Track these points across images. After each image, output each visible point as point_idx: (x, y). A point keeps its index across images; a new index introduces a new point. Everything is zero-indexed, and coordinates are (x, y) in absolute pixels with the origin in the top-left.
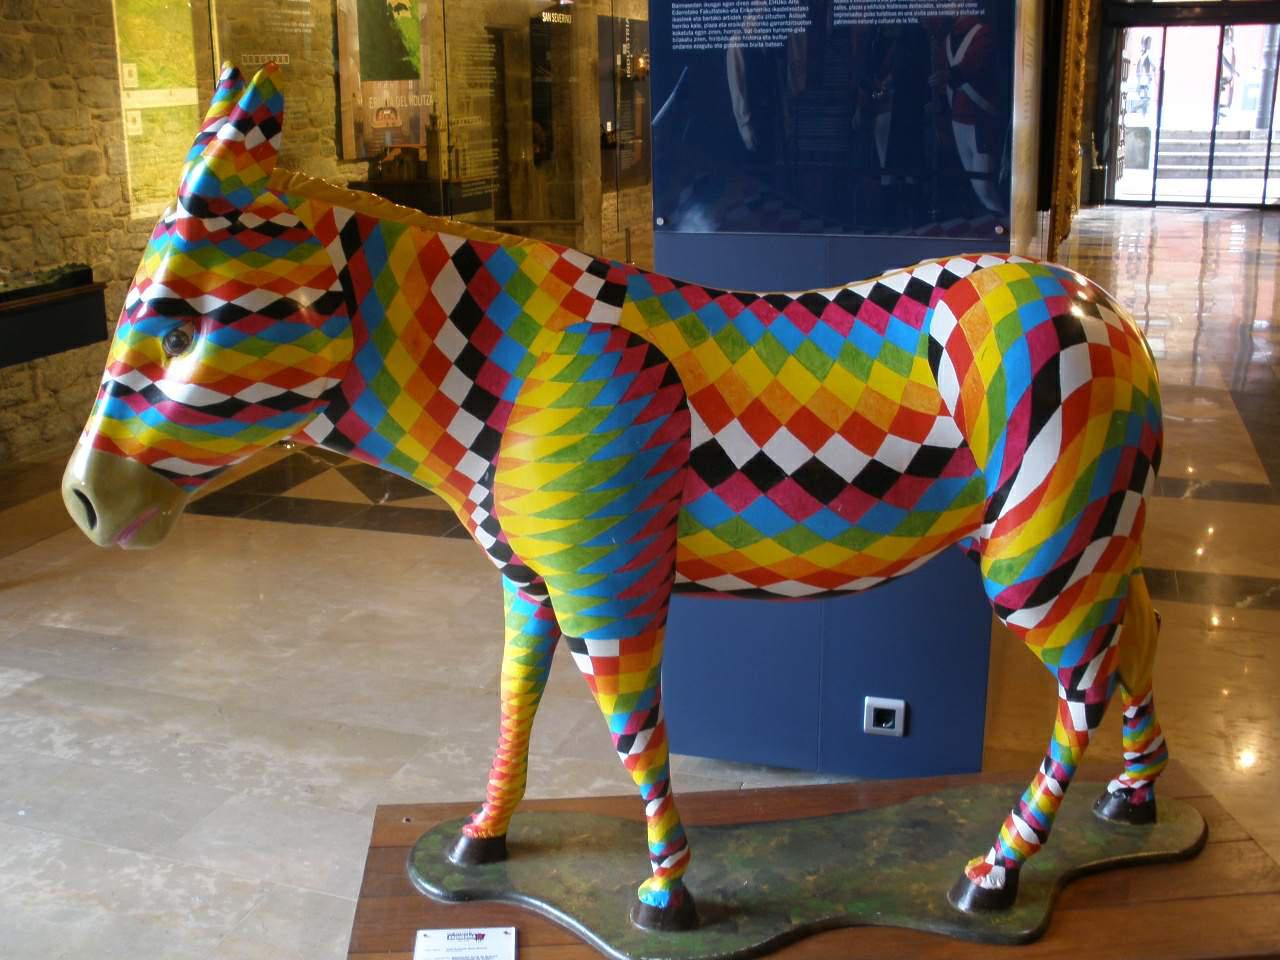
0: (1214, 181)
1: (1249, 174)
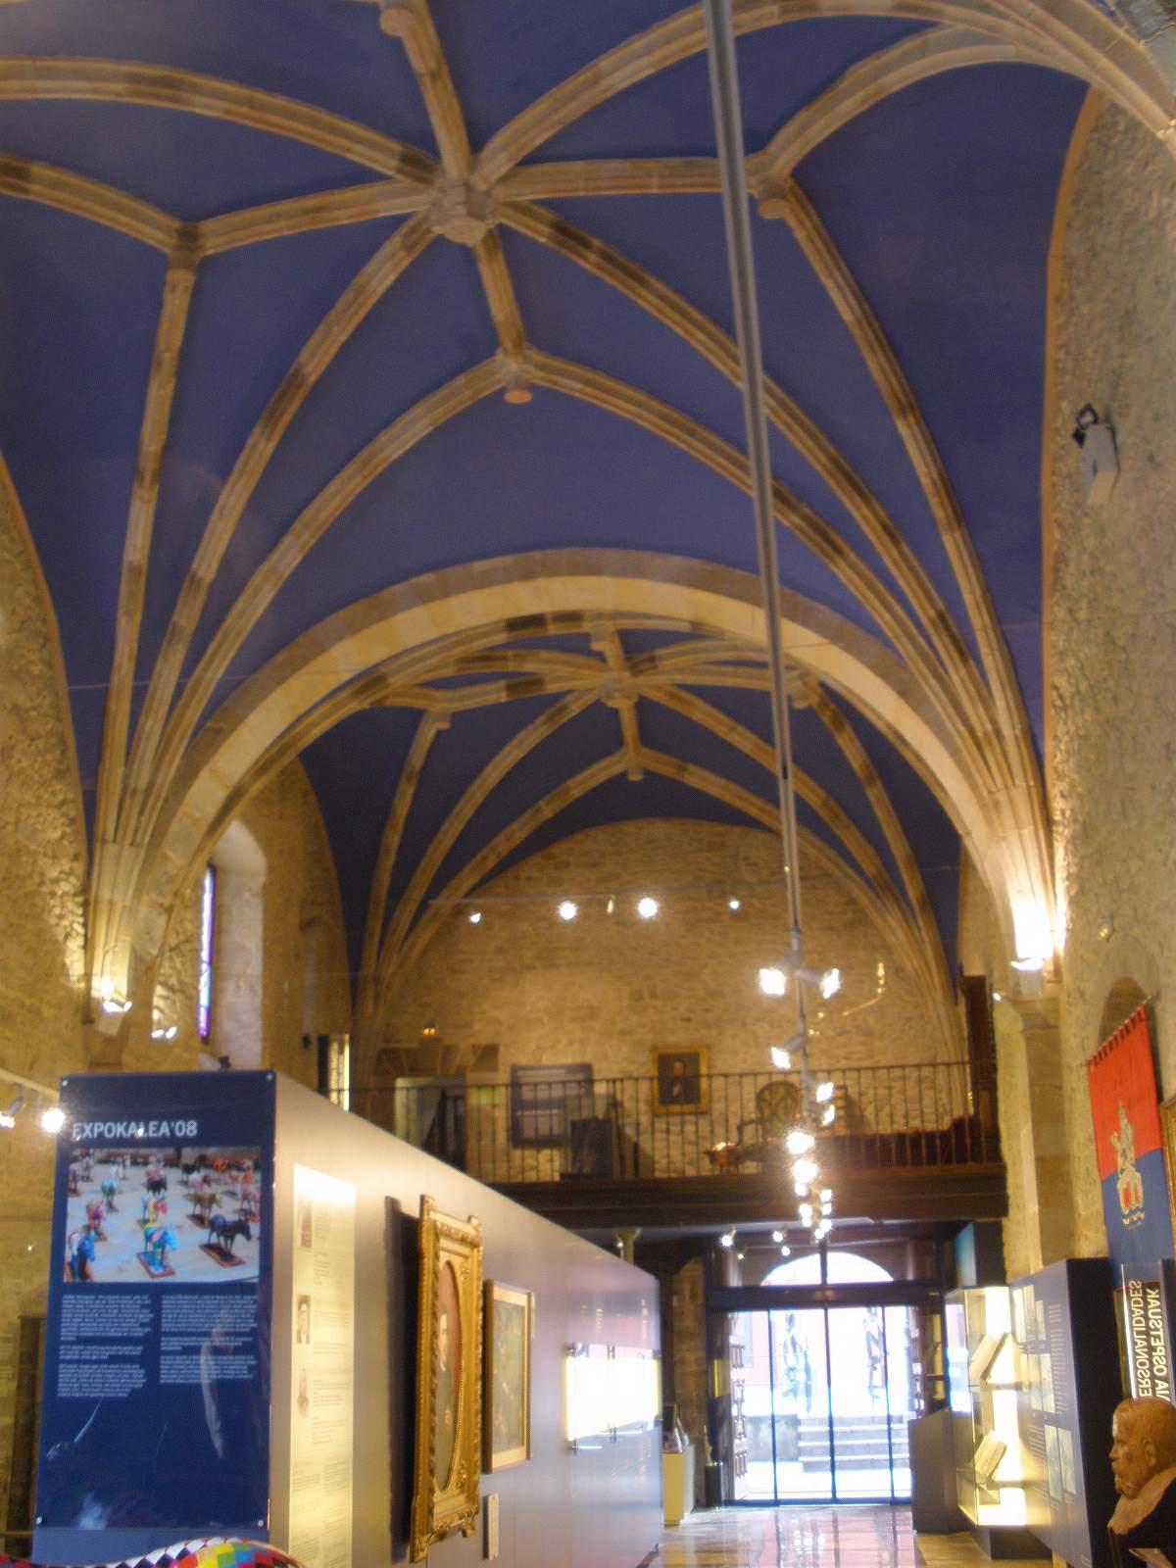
0: (837, 1473)
1: (873, 1465)
